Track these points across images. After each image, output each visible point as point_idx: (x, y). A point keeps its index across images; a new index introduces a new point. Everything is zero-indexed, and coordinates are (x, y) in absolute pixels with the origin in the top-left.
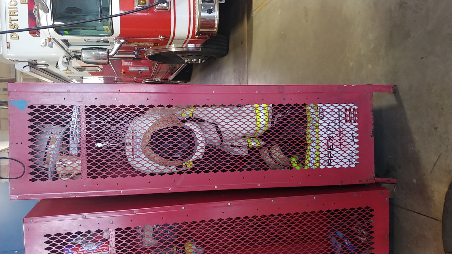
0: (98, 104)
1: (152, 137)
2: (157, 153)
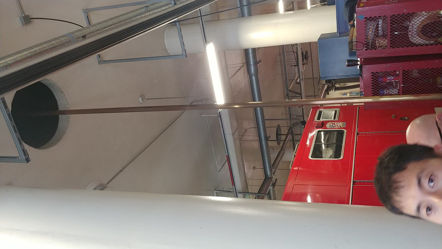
0: (396, 14)
1: (423, 28)
2: (425, 35)
